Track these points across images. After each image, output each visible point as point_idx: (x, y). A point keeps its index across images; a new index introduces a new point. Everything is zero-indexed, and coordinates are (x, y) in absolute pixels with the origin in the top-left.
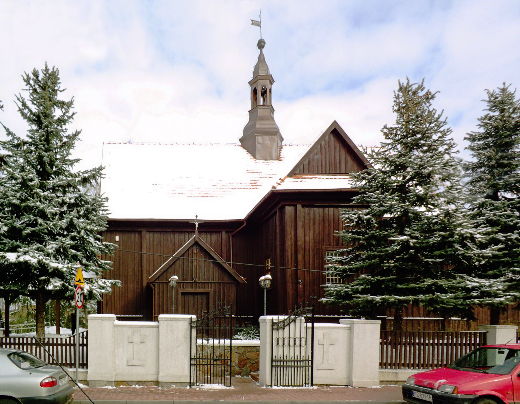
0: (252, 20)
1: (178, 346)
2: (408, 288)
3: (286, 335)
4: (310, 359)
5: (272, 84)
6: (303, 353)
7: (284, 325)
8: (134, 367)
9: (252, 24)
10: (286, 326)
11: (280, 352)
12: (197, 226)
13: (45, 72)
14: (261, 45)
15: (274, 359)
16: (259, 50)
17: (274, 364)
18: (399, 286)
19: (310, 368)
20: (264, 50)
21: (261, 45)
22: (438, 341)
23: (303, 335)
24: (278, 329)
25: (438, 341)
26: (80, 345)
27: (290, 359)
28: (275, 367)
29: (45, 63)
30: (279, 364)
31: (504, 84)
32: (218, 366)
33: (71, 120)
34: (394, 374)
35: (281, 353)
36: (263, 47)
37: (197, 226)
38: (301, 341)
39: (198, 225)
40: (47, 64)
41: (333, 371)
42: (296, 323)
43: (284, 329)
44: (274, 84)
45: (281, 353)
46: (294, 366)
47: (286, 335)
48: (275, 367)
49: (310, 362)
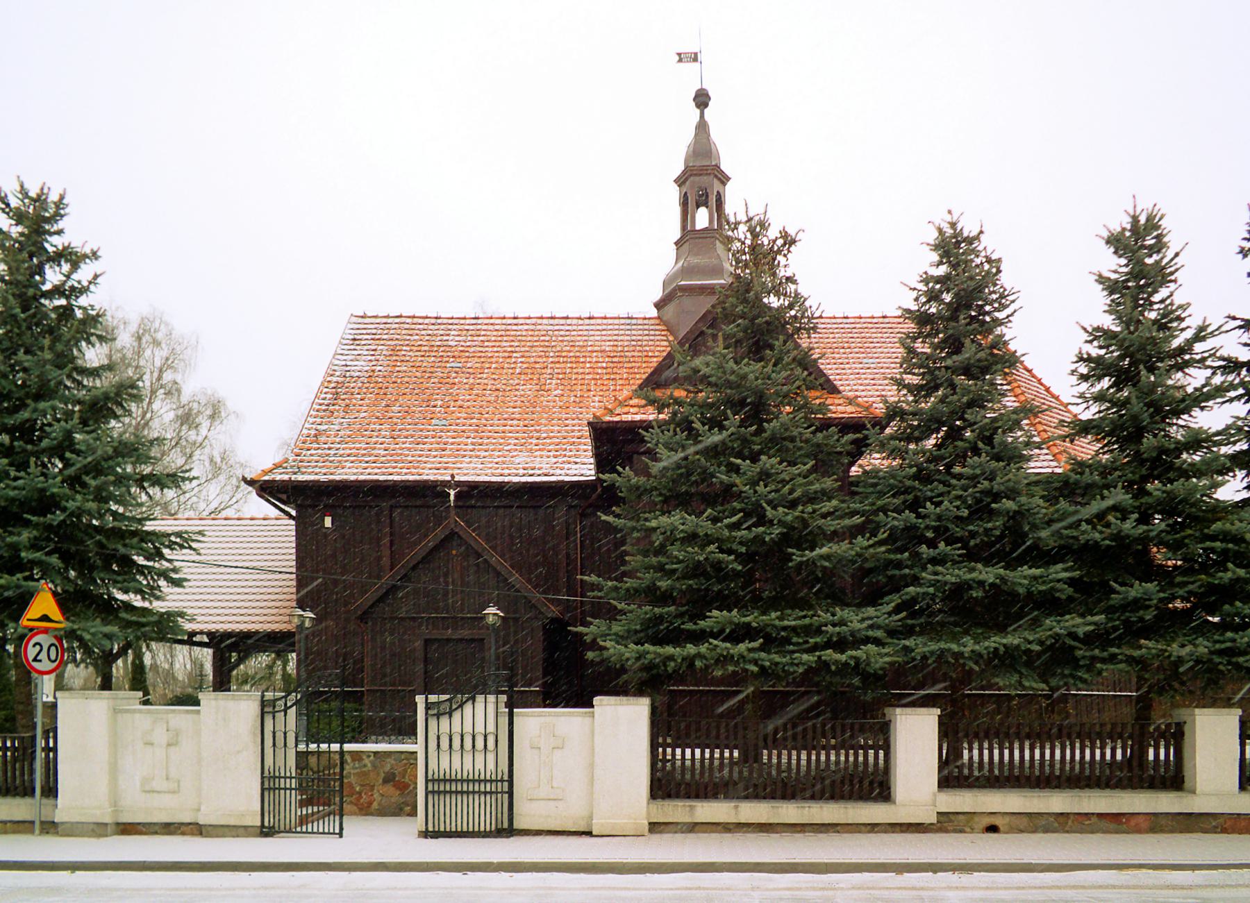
0: (679, 54)
1: (239, 752)
2: (695, 631)
3: (456, 728)
4: (506, 778)
5: (724, 184)
6: (486, 764)
7: (286, 704)
8: (155, 794)
9: (680, 60)
10: (456, 709)
11: (445, 764)
12: (452, 498)
13: (20, 196)
14: (702, 99)
15: (430, 777)
16: (698, 111)
17: (430, 788)
18: (1210, 619)
19: (506, 796)
20: (706, 111)
21: (702, 99)
22: (665, 740)
23: (491, 728)
24: (438, 716)
25: (665, 740)
26: (43, 749)
27: (453, 777)
28: (433, 792)
29: (16, 178)
30: (448, 788)
31: (950, 212)
32: (499, 795)
33: (92, 287)
34: (688, 809)
35: (445, 764)
36: (706, 105)
37: (452, 498)
38: (485, 741)
39: (456, 496)
40: (21, 179)
41: (560, 802)
42: (476, 704)
43: (450, 717)
44: (729, 186)
45: (445, 764)
46: (462, 792)
47: (456, 728)
48: (433, 792)
49: (506, 784)
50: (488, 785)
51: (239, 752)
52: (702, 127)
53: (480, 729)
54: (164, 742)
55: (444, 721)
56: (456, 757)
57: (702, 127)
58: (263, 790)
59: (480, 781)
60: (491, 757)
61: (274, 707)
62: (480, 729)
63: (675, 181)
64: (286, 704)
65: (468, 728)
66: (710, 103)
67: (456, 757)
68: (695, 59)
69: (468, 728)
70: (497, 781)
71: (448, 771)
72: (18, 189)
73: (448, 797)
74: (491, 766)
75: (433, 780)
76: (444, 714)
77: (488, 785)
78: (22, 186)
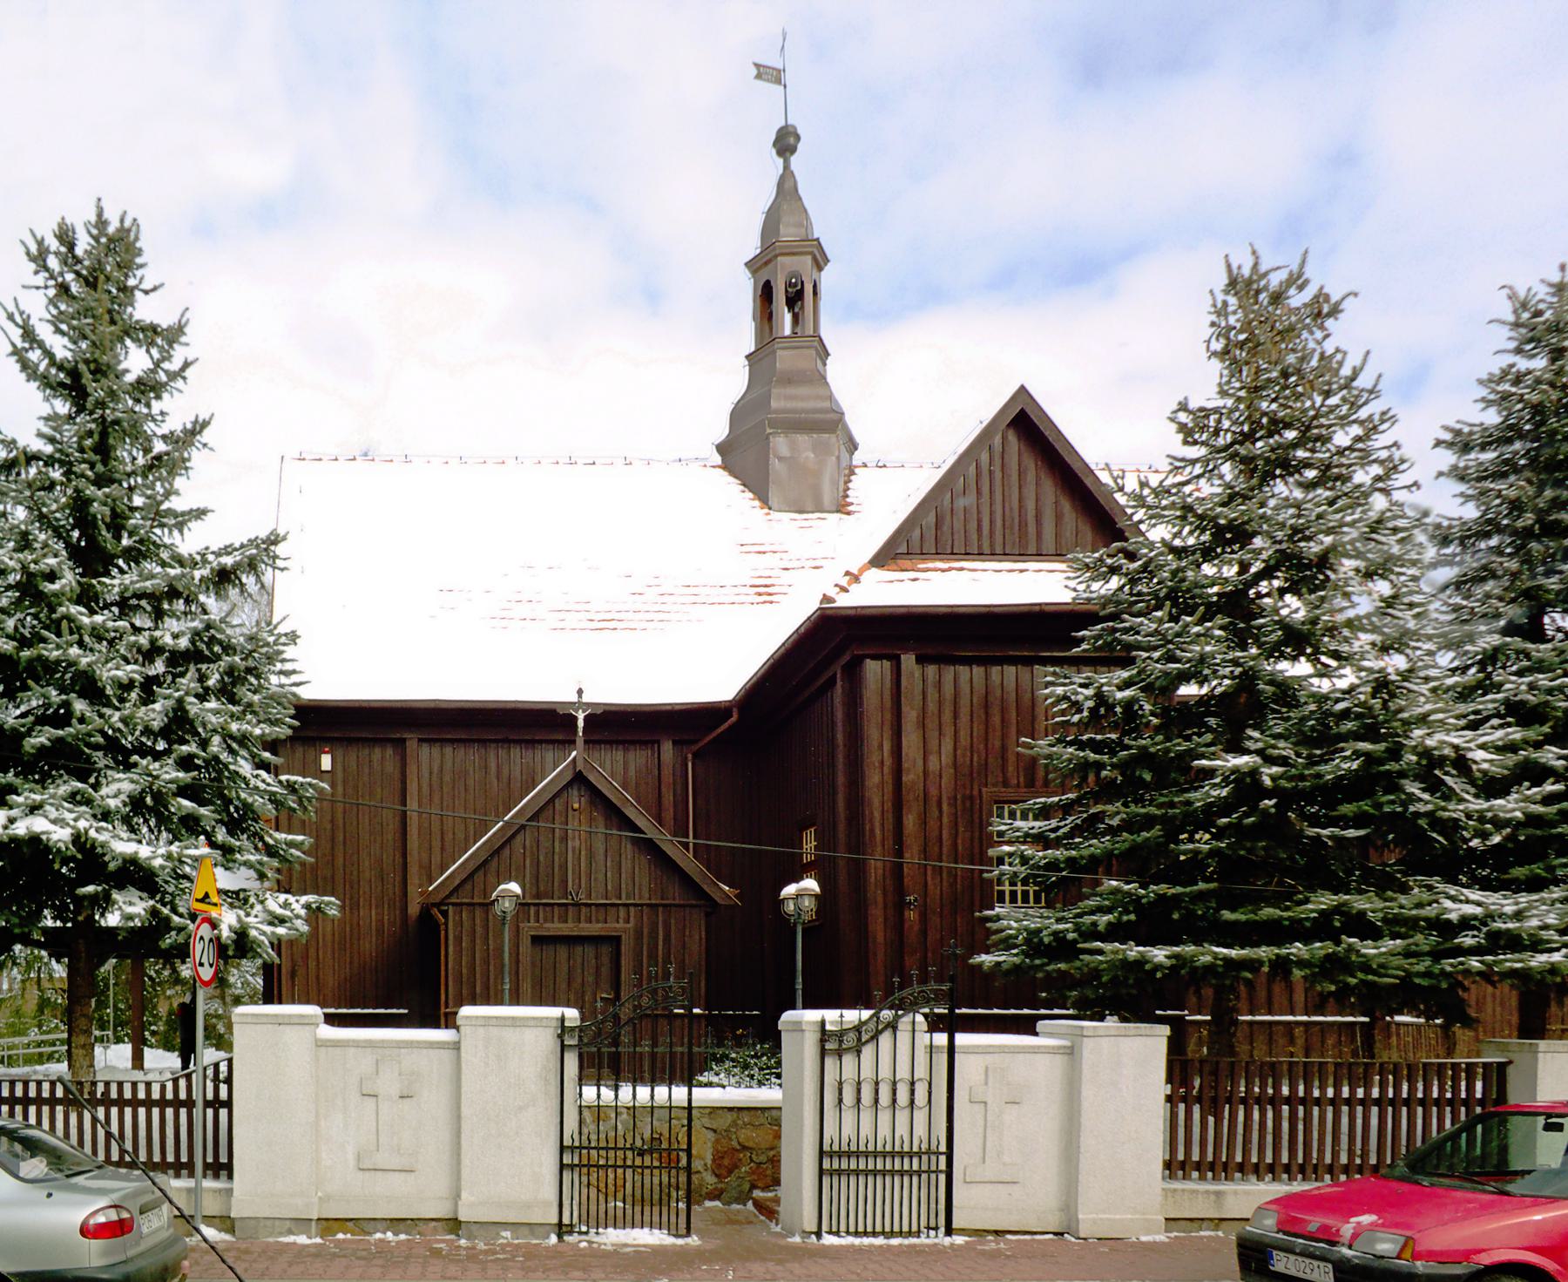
1: (521, 1108)
4: (943, 1148)
6: (921, 1129)
7: (859, 1039)
8: (379, 1174)
11: (847, 1128)
12: (581, 723)
13: (95, 232)
14: (786, 143)
15: (826, 1148)
16: (781, 161)
17: (826, 1165)
19: (942, 1177)
21: (786, 143)
22: (1352, 1092)
23: (922, 1072)
24: (839, 1054)
26: (207, 1104)
28: (831, 1173)
32: (629, 1172)
34: (1213, 1197)
36: (793, 150)
37: (581, 723)
38: (912, 1092)
39: (586, 719)
40: (104, 204)
43: (859, 1052)
48: (831, 1173)
49: (943, 1159)
50: (879, 1161)
51: (521, 1108)
52: (787, 189)
53: (903, 1073)
54: (395, 1091)
55: (849, 1060)
56: (866, 1117)
57: (787, 189)
58: (562, 1167)
59: (902, 1155)
60: (920, 1117)
61: (841, 1042)
62: (903, 1073)
63: (746, 264)
64: (859, 1039)
65: (885, 1072)
66: (800, 146)
67: (866, 1117)
68: (778, 81)
69: (885, 1072)
70: (607, 1149)
71: (854, 1140)
72: (93, 219)
73: (844, 1179)
74: (920, 1130)
75: (831, 1154)
76: (848, 1050)
77: (879, 1161)
78: (100, 214)
